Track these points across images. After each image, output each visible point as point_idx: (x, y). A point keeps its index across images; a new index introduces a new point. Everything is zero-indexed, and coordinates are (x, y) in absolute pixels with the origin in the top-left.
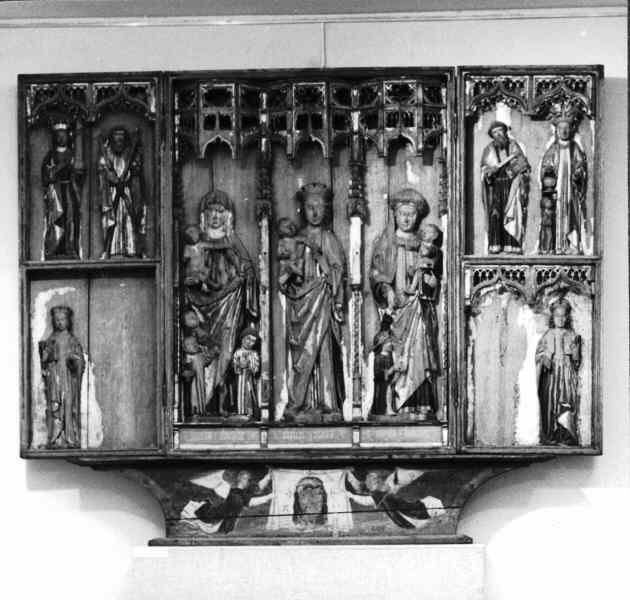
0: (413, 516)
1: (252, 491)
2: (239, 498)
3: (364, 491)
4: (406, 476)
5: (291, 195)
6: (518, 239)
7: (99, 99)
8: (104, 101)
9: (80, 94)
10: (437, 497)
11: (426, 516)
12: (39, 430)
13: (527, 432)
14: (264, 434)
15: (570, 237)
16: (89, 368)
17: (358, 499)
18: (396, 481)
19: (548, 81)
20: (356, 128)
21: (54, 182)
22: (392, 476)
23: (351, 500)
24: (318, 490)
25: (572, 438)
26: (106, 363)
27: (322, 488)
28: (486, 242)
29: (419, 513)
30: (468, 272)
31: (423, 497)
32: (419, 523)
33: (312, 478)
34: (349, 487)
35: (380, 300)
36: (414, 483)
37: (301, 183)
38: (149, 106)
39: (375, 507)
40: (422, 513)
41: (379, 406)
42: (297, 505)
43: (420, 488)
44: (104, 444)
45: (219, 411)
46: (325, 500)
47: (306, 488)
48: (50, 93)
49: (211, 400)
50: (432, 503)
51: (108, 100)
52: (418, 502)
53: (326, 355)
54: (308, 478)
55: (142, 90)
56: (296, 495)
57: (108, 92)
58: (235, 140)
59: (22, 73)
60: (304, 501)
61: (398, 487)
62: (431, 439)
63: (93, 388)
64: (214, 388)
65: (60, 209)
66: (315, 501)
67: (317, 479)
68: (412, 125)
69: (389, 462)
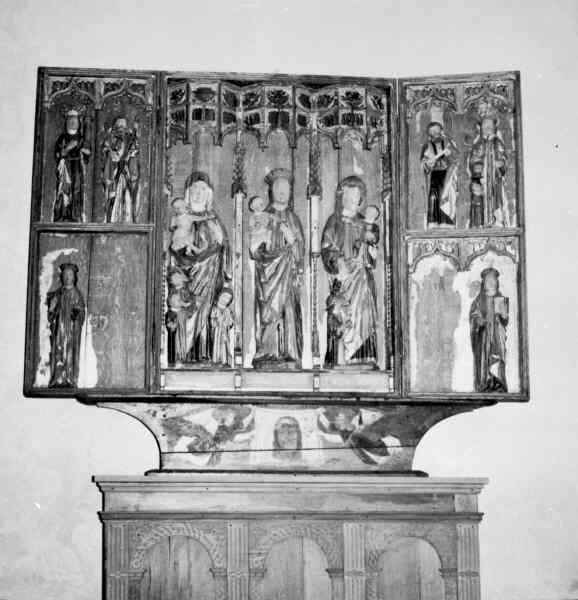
0: (375, 453)
1: (237, 427)
2: (225, 433)
3: (334, 428)
4: (369, 416)
5: (260, 178)
6: (452, 218)
7: (106, 91)
8: (109, 94)
9: (91, 87)
10: (395, 436)
11: (385, 454)
12: (321, 505)
13: (463, 382)
14: (238, 378)
15: (496, 214)
16: (88, 319)
17: (328, 437)
18: (361, 422)
19: (473, 87)
20: (315, 127)
21: (65, 157)
22: (358, 417)
23: (323, 439)
24: (293, 429)
25: (498, 385)
26: (338, 148)
27: (297, 426)
28: (426, 221)
29: (380, 450)
30: (411, 245)
31: (384, 436)
32: (381, 460)
33: (289, 418)
34: (321, 426)
35: (331, 268)
36: (375, 424)
37: (267, 170)
38: (147, 99)
39: (344, 445)
40: (382, 449)
41: (331, 358)
42: (276, 442)
43: (381, 428)
44: (101, 380)
45: (200, 354)
46: (300, 438)
47: (283, 426)
48: (63, 85)
49: (192, 350)
50: (390, 441)
51: (113, 93)
52: (380, 440)
53: (290, 312)
54: (286, 418)
55: (143, 86)
56: (276, 433)
57: (114, 86)
58: (217, 129)
59: (43, 65)
60: (282, 437)
61: (362, 427)
62: (379, 384)
63: (90, 336)
64: (194, 337)
65: (68, 180)
66: (291, 438)
67: (293, 419)
68: (362, 124)
69: (356, 401)
